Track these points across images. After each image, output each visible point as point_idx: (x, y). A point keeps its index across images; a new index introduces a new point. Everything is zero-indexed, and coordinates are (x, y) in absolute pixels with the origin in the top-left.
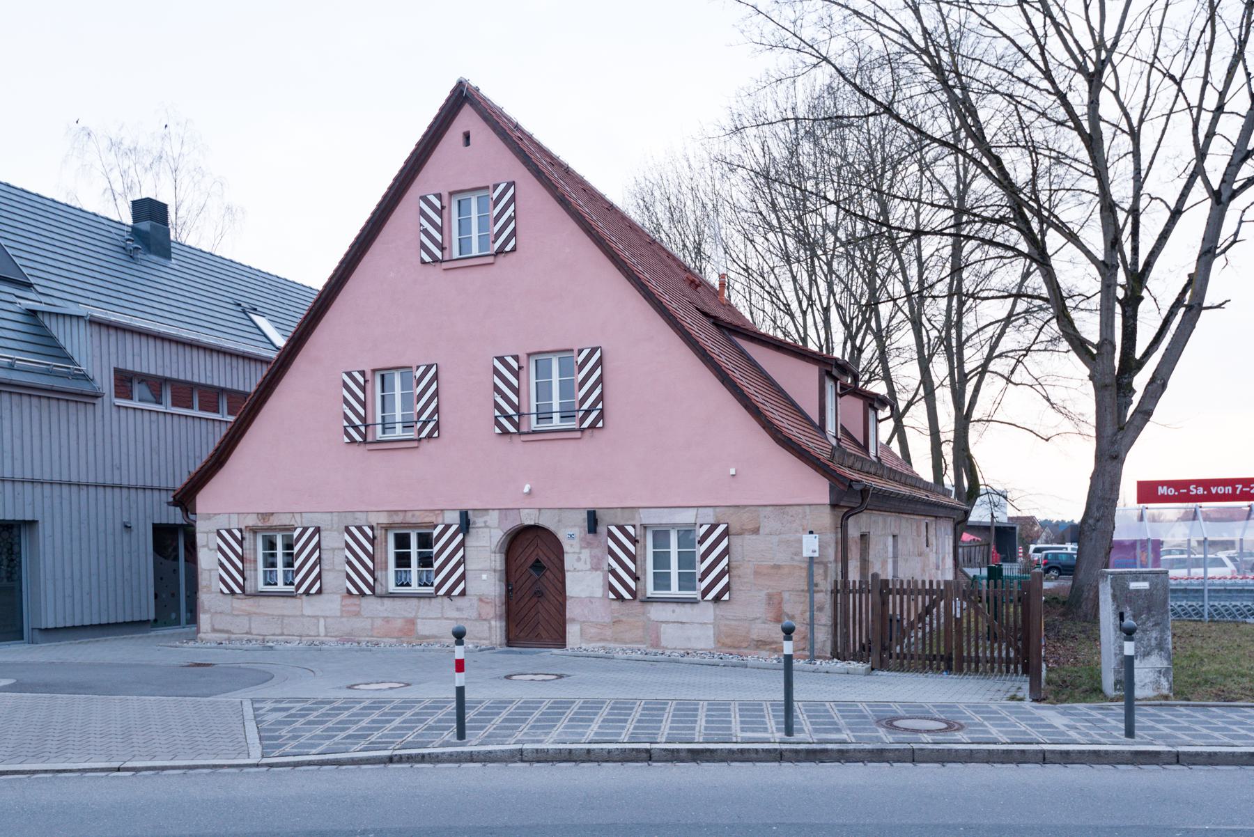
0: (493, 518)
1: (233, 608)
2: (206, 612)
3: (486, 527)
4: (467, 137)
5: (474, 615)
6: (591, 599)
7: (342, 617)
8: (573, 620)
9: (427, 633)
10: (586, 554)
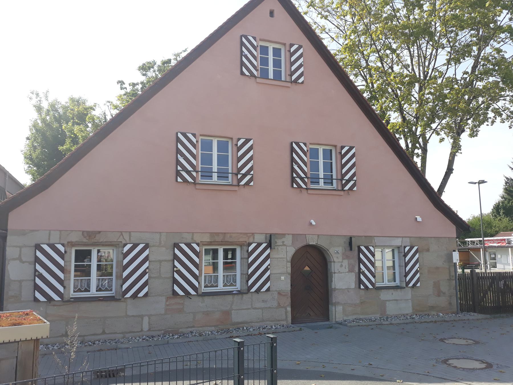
0: (288, 240)
4: (272, 14)
5: (275, 304)
6: (348, 289)
8: (338, 303)
9: (240, 320)
10: (346, 263)
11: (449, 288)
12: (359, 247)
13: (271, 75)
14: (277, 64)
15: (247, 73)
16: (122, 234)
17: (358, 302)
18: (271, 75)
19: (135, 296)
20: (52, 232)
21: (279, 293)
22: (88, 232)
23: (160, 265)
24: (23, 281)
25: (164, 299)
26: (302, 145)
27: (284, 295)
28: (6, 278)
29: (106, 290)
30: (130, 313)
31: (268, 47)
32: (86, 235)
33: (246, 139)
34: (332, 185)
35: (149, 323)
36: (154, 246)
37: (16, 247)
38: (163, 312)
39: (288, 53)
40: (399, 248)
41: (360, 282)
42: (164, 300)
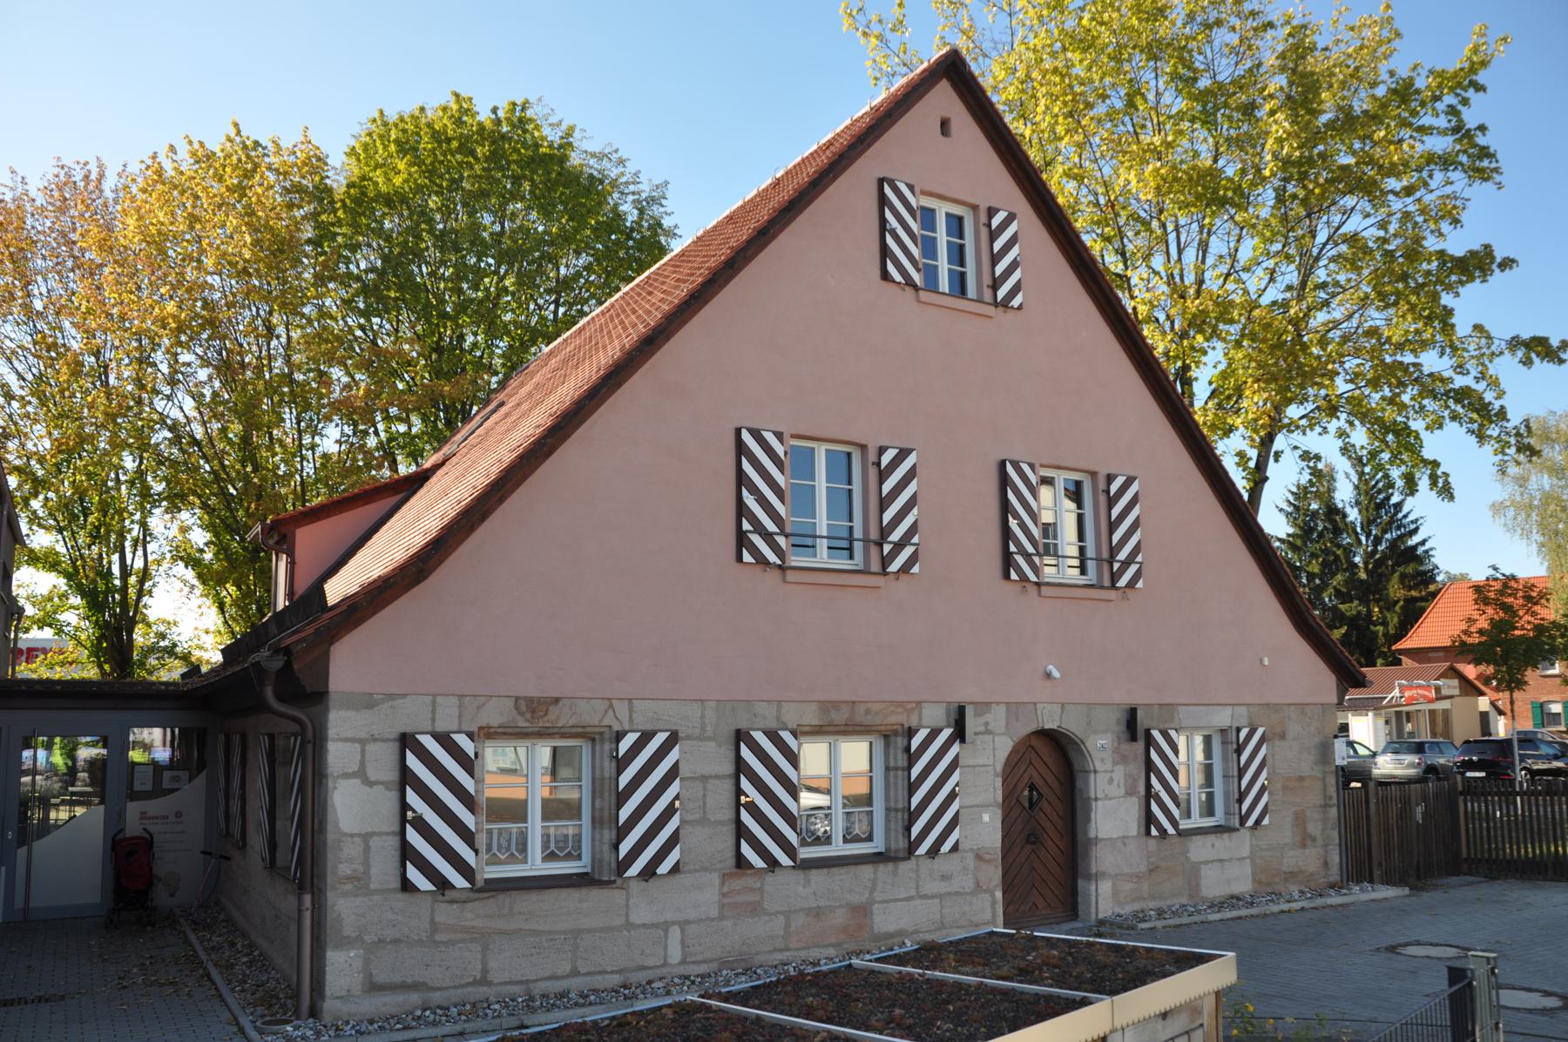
0: (997, 718)
1: (435, 927)
2: (345, 943)
3: (988, 732)
4: (945, 126)
5: (969, 884)
7: (721, 917)
10: (1119, 773)
11: (1325, 827)
12: (1148, 733)
13: (944, 285)
14: (958, 255)
15: (898, 277)
16: (611, 706)
17: (1143, 868)
18: (944, 285)
19: (649, 872)
20: (439, 700)
21: (978, 857)
22: (529, 700)
23: (705, 789)
24: (373, 834)
25: (715, 878)
26: (1025, 467)
27: (989, 861)
28: (330, 827)
29: (569, 857)
30: (637, 917)
31: (933, 211)
32: (523, 707)
33: (901, 450)
34: (851, 558)
35: (683, 943)
36: (689, 738)
37: (352, 740)
38: (714, 913)
39: (984, 232)
40: (1223, 731)
41: (1149, 819)
42: (717, 882)
